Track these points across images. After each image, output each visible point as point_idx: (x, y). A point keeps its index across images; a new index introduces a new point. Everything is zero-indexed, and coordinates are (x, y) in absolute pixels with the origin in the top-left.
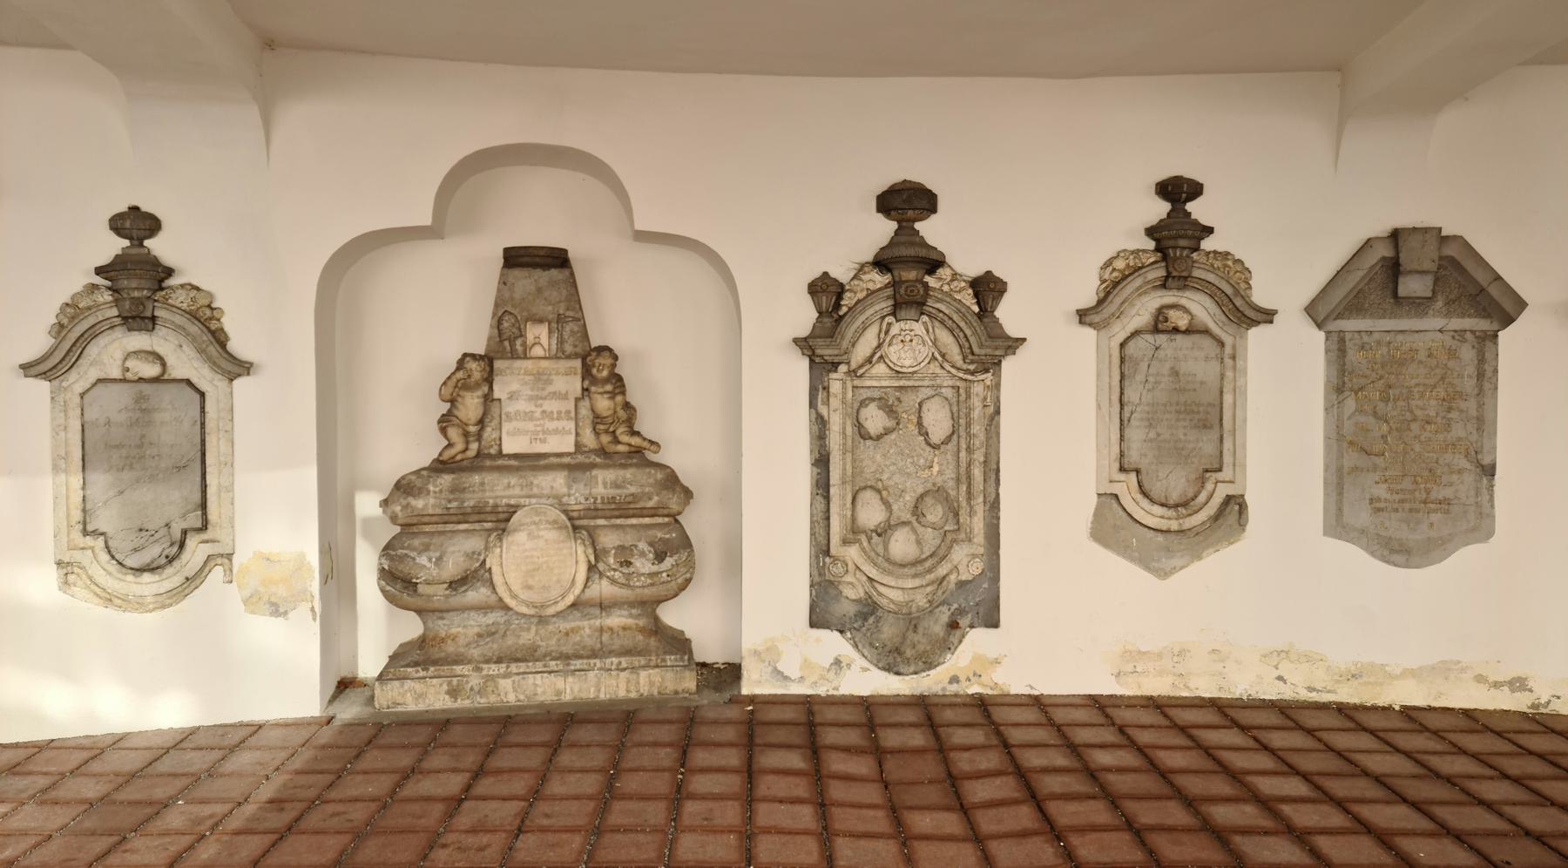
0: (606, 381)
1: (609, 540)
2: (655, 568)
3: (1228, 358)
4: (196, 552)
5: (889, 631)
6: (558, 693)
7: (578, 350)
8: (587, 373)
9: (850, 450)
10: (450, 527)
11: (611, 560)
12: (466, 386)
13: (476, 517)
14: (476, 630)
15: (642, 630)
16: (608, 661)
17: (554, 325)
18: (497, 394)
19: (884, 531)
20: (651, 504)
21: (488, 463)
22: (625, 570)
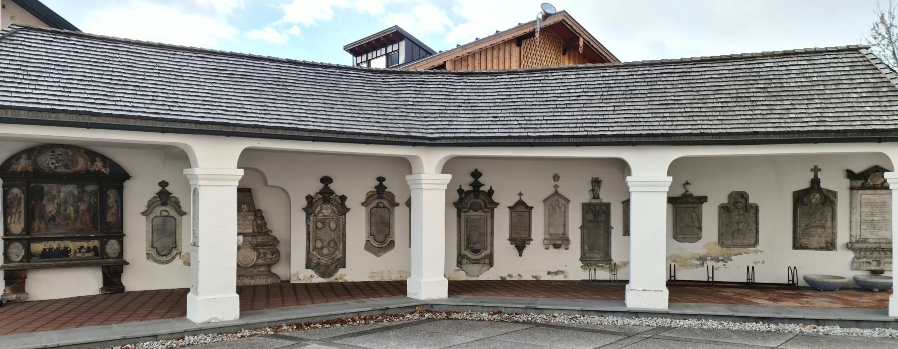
1: (262, 251)
3: (391, 213)
4: (174, 252)
5: (322, 269)
8: (255, 215)
9: (315, 231)
19: (322, 248)
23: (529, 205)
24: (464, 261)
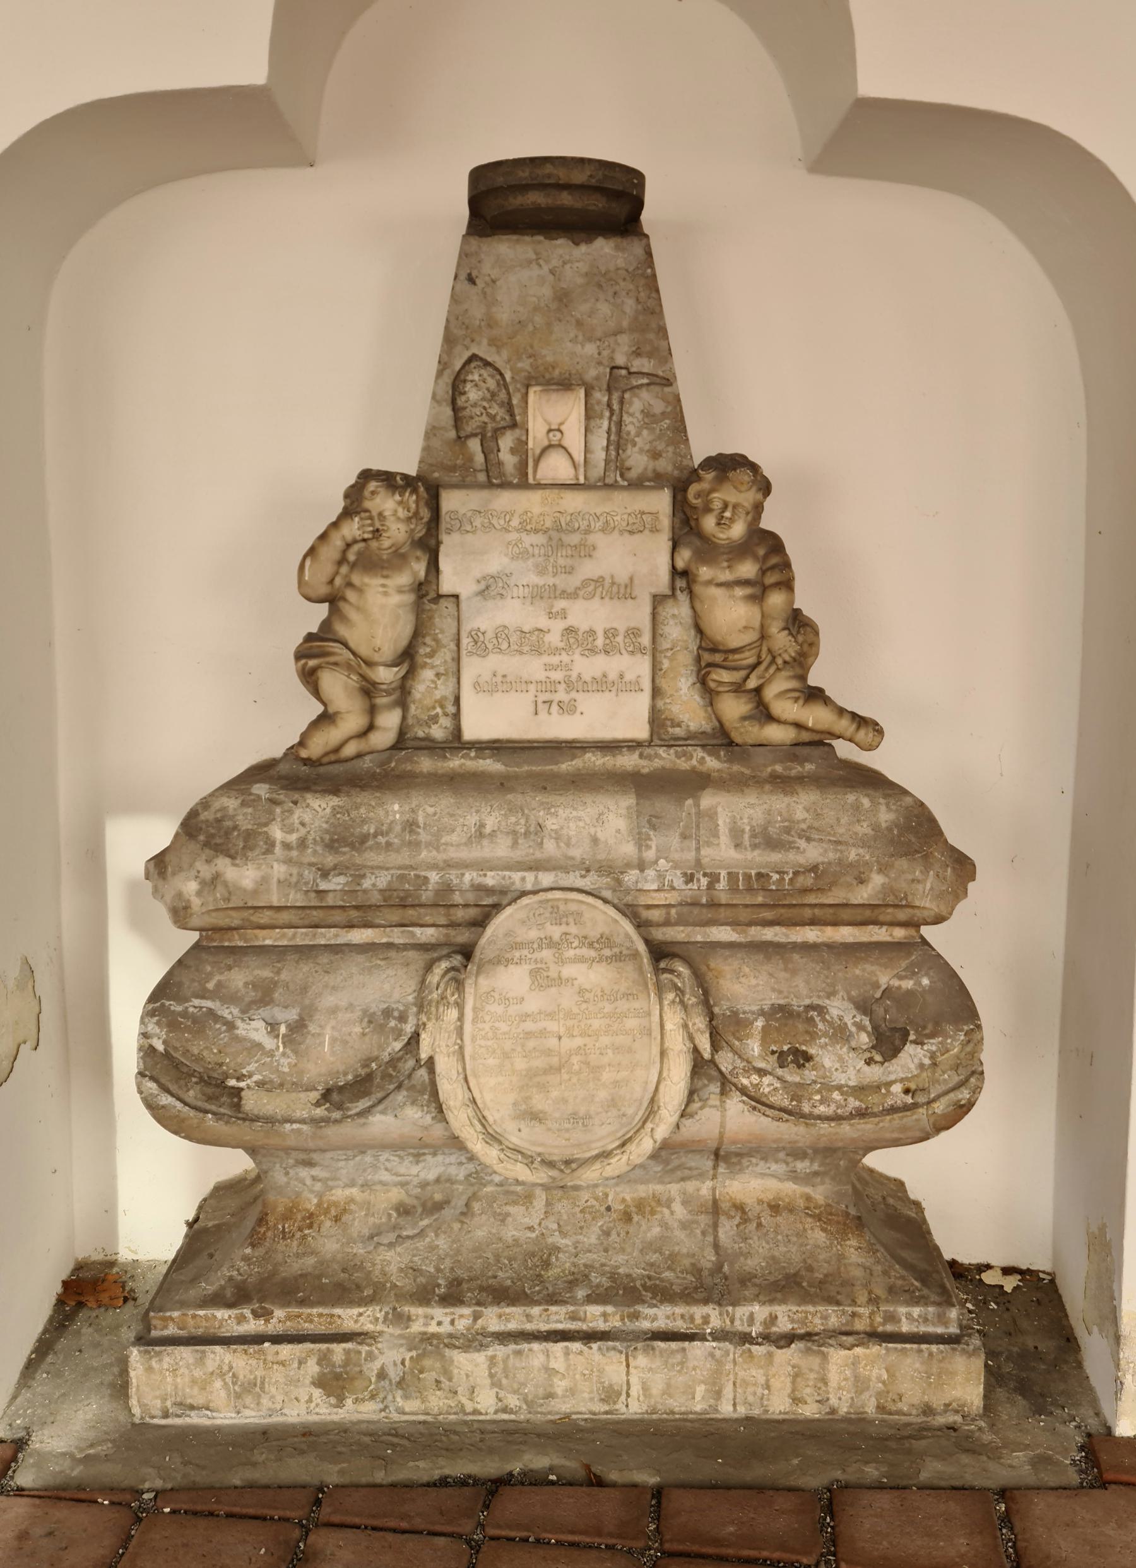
0: (740, 550)
1: (747, 987)
2: (874, 1073)
6: (610, 1395)
7: (664, 465)
8: (686, 525)
10: (326, 936)
11: (754, 1047)
12: (367, 559)
13: (395, 916)
14: (396, 1195)
15: (823, 1216)
16: (741, 1312)
17: (601, 397)
18: (450, 580)
20: (863, 895)
21: (426, 764)
22: (792, 1076)
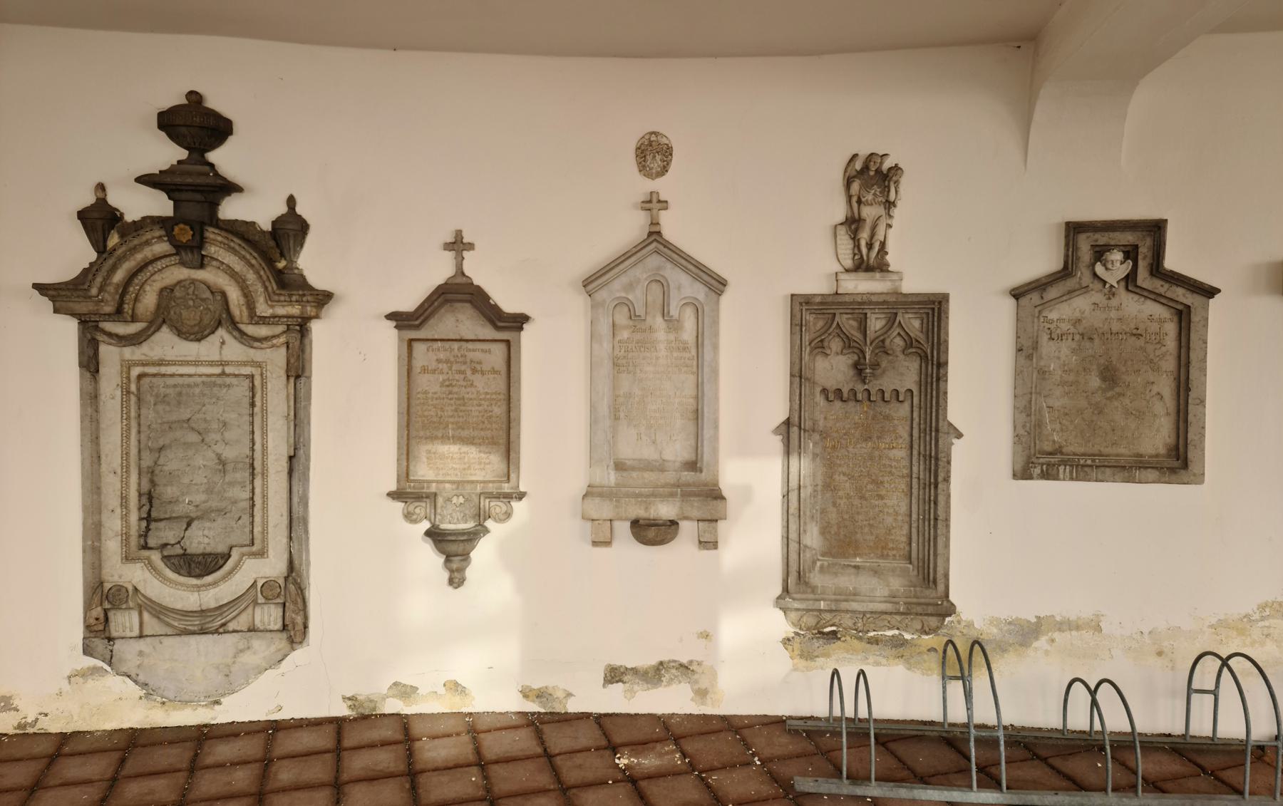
23: (509, 305)
24: (125, 622)
